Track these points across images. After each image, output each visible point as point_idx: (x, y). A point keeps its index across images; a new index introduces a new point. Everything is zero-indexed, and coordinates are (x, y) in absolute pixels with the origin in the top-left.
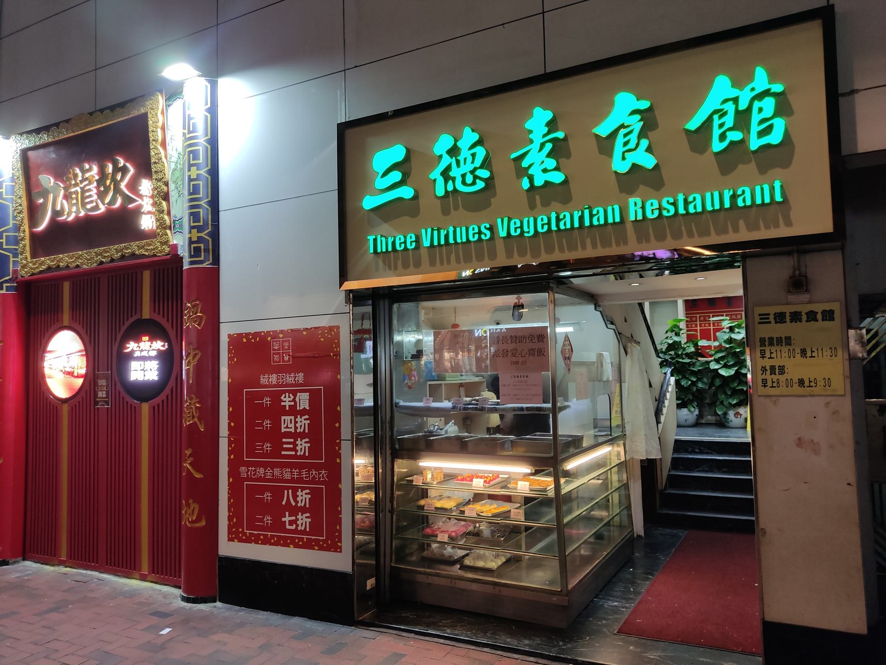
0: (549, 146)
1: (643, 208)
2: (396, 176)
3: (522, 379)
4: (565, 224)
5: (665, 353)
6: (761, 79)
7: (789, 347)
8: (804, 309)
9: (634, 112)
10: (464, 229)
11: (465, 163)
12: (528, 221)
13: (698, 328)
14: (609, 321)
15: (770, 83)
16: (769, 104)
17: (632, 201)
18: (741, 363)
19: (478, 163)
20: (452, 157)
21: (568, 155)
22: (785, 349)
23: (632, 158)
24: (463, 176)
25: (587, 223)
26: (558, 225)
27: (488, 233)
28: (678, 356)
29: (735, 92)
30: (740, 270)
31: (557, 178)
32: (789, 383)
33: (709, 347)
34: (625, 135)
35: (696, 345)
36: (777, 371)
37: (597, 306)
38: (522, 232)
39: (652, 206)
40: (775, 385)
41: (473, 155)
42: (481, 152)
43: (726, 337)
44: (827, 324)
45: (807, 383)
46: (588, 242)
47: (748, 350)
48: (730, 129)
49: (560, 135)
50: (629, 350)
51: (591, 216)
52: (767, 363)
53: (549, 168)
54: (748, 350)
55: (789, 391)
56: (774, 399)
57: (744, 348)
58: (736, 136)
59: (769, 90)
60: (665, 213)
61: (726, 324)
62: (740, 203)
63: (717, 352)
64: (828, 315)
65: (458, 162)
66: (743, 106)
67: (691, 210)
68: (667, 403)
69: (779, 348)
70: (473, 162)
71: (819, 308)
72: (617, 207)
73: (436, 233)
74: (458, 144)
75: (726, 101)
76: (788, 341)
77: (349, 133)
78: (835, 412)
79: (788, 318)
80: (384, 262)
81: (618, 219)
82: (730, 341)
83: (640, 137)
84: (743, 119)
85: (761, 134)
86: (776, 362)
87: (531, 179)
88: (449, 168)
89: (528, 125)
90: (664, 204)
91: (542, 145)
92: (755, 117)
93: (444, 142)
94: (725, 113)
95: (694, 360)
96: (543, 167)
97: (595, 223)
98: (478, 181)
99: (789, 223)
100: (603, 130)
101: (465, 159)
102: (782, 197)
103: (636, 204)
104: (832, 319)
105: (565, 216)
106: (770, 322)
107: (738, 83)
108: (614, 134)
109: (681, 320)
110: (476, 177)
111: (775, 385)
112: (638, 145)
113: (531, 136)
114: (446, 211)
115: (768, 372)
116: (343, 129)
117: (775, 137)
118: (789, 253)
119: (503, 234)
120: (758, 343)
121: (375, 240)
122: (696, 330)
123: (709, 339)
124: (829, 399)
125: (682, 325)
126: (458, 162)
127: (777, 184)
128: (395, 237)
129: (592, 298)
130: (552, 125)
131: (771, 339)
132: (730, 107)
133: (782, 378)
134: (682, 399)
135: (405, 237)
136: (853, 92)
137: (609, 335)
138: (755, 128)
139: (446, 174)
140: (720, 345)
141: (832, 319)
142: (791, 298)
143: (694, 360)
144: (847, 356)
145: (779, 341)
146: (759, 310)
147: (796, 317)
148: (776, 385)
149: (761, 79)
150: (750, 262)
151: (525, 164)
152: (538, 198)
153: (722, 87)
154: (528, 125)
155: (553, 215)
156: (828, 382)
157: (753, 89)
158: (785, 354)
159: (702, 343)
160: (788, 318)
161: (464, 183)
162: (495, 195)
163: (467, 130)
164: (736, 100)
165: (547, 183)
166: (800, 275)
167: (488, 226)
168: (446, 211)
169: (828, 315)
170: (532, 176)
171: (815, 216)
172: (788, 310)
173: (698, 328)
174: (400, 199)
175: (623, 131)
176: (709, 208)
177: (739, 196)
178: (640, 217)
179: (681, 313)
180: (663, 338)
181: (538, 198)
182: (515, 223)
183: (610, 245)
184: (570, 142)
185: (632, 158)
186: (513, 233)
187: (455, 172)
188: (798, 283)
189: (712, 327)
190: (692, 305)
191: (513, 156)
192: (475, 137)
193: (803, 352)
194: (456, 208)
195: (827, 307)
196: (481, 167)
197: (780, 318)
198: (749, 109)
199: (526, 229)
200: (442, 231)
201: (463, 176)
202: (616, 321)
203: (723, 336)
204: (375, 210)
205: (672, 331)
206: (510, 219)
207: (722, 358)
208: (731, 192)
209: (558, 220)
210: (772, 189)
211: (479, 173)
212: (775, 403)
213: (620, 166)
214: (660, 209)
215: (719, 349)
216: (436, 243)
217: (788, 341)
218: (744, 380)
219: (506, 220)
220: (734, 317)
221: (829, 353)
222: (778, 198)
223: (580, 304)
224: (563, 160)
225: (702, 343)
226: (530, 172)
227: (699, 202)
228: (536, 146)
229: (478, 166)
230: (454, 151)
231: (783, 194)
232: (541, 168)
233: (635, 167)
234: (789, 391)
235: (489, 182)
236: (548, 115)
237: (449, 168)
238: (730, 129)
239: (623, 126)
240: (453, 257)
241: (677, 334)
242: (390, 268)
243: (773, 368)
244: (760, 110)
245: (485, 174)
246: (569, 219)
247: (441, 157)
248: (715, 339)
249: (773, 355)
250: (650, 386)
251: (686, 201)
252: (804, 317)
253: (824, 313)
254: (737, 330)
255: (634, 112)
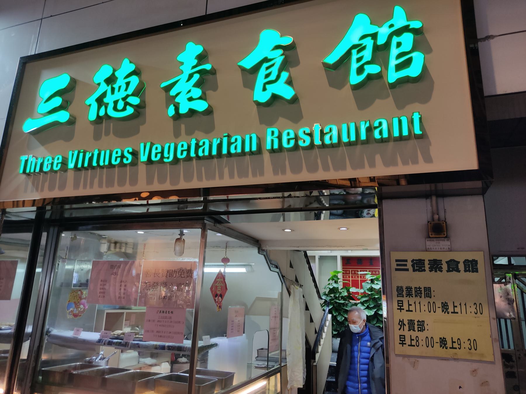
0: (197, 77)
1: (280, 138)
2: (58, 101)
3: (167, 315)
4: (203, 151)
5: (327, 295)
6: (399, 17)
7: (428, 299)
8: (445, 257)
9: (277, 47)
10: (108, 152)
11: (119, 91)
12: (169, 147)
13: (351, 279)
14: (272, 264)
15: (408, 20)
16: (407, 39)
17: (269, 131)
18: (379, 307)
19: (131, 90)
20: (108, 85)
21: (215, 88)
22: (424, 301)
23: (272, 89)
24: (116, 103)
25: (225, 151)
26: (196, 152)
27: (130, 157)
28: (336, 298)
29: (373, 29)
30: (375, 221)
31: (201, 106)
32: (430, 342)
33: (357, 293)
34: (267, 68)
35: (348, 291)
36: (416, 327)
37: (261, 250)
38: (162, 157)
39: (288, 134)
40: (414, 343)
41: (128, 84)
42: (135, 81)
43: (369, 286)
44: (470, 275)
45: (449, 344)
46: (226, 171)
47: (384, 298)
48: (368, 63)
49: (208, 67)
50: (292, 291)
51: (229, 144)
52: (406, 316)
53: (194, 97)
54: (384, 298)
55: (429, 351)
56: (412, 360)
57: (381, 295)
58: (373, 69)
59: (408, 26)
60: (301, 143)
61: (369, 277)
62: (376, 135)
63: (362, 297)
64: (471, 266)
65: (113, 90)
66: (381, 41)
67: (327, 141)
68: (324, 335)
69: (418, 300)
70: (126, 90)
71: (460, 257)
72: (254, 136)
73: (81, 155)
74: (117, 74)
75: (363, 37)
76: (428, 292)
77: (29, 66)
78: (484, 383)
79: (427, 266)
80: (33, 184)
81: (254, 148)
82: (371, 289)
83: (280, 71)
84: (381, 52)
85: (399, 67)
86: (416, 316)
87: (177, 108)
88: (104, 95)
89: (180, 58)
90: (301, 134)
91: (191, 76)
92: (394, 51)
93: (106, 71)
94: (364, 48)
95: (347, 302)
96: (189, 95)
97: (233, 151)
98: (128, 107)
99: (428, 159)
100: (248, 63)
101: (120, 87)
102: (421, 130)
103: (273, 133)
104: (475, 270)
105: (204, 143)
106: (407, 270)
107: (376, 21)
108: (256, 68)
109: (338, 272)
110: (127, 104)
111: (414, 343)
112: (278, 77)
113: (181, 68)
114: (97, 136)
115: (406, 328)
116: (26, 62)
117: (414, 71)
118: (426, 196)
119: (143, 158)
120: (395, 293)
121: (26, 161)
122: (349, 280)
123: (357, 287)
124: (475, 366)
125: (340, 276)
126: (113, 90)
127: (416, 117)
128: (44, 158)
129: (257, 243)
130: (202, 58)
131: (409, 289)
132: (369, 42)
133: (422, 336)
134: (338, 331)
135: (53, 159)
136: (489, 37)
137: (274, 277)
138: (393, 62)
139: (100, 101)
140: (365, 292)
141: (475, 270)
142: (430, 244)
143: (347, 302)
144: (493, 315)
145: (418, 292)
146: (396, 255)
147: (435, 265)
148: (415, 343)
149: (399, 17)
150: (387, 204)
151: (173, 93)
152: (183, 127)
153: (360, 25)
154: (180, 58)
155: (193, 142)
156: (473, 345)
157: (391, 26)
158: (425, 308)
159: (353, 290)
160: (427, 266)
161: (115, 109)
162: (144, 123)
163: (126, 61)
164: (374, 36)
165: (192, 112)
166: (439, 219)
167: (131, 150)
168: (97, 136)
169: (471, 266)
170: (178, 103)
171: (457, 151)
172: (427, 257)
173: (351, 279)
174: (56, 124)
175: (265, 65)
176: (345, 139)
177: (376, 128)
178: (276, 146)
179: (340, 268)
180: (325, 285)
181: (183, 127)
182: (157, 148)
183: (247, 176)
184: (219, 76)
185: (272, 89)
186: (153, 158)
187: (109, 99)
188: (438, 229)
189: (351, 275)
190: (347, 261)
191: (164, 85)
192: (132, 67)
193: (445, 307)
194: (107, 134)
195: (470, 256)
196: (133, 95)
197: (418, 265)
198: (387, 45)
199: (166, 155)
200: (87, 153)
201: (116, 103)
202: (280, 266)
203: (367, 285)
204: (35, 133)
205: (333, 279)
206: (152, 145)
207: (366, 302)
208: (368, 125)
209: (197, 146)
210: (411, 122)
211: (129, 100)
212: (414, 365)
213: (261, 96)
214: (296, 138)
215: (364, 295)
216: (79, 166)
217: (428, 292)
218: (381, 319)
219: (148, 145)
220: (374, 273)
221: (473, 309)
222: (417, 131)
223: (247, 247)
224: (209, 93)
225: (353, 290)
226: (177, 100)
227: (335, 133)
228: (185, 76)
229: (130, 93)
230: (111, 80)
231: (422, 128)
232: (187, 96)
233: (275, 97)
234: (429, 351)
235: (139, 109)
236: (199, 49)
237: (104, 95)
238: (368, 63)
239: (266, 60)
240: (96, 180)
241: (336, 282)
242: (37, 190)
243: (411, 323)
244: (399, 45)
245: (135, 101)
246: (208, 145)
247: (99, 84)
248: (362, 288)
249: (412, 308)
250: (312, 321)
251: (322, 132)
252: (445, 267)
253: (466, 262)
254: (376, 282)
255: (277, 47)
